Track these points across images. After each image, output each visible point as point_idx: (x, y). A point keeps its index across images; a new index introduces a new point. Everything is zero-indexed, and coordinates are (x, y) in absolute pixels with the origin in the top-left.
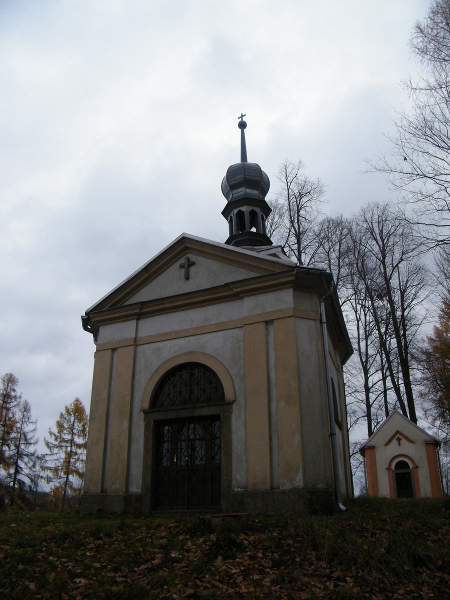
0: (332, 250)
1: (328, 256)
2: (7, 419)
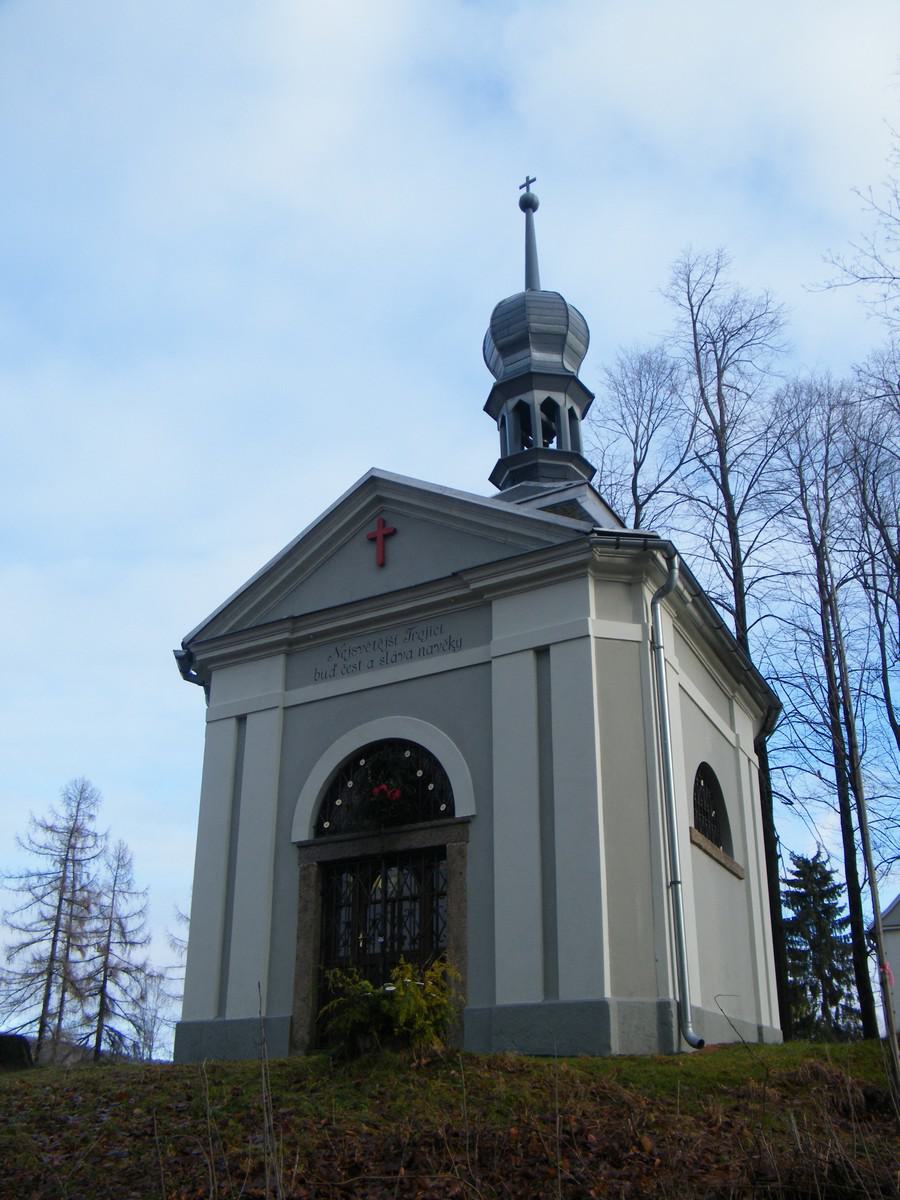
0: (807, 460)
1: (800, 475)
2: (78, 887)
